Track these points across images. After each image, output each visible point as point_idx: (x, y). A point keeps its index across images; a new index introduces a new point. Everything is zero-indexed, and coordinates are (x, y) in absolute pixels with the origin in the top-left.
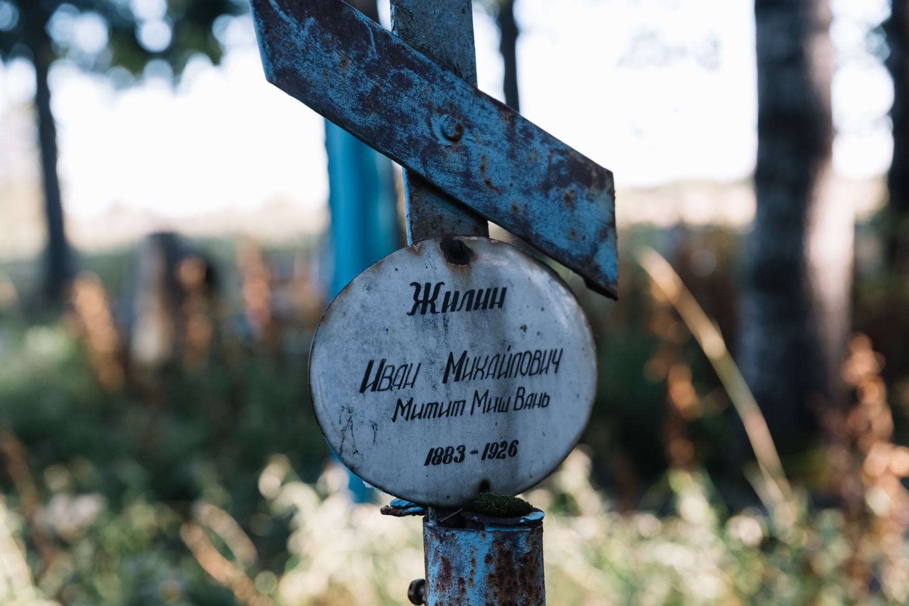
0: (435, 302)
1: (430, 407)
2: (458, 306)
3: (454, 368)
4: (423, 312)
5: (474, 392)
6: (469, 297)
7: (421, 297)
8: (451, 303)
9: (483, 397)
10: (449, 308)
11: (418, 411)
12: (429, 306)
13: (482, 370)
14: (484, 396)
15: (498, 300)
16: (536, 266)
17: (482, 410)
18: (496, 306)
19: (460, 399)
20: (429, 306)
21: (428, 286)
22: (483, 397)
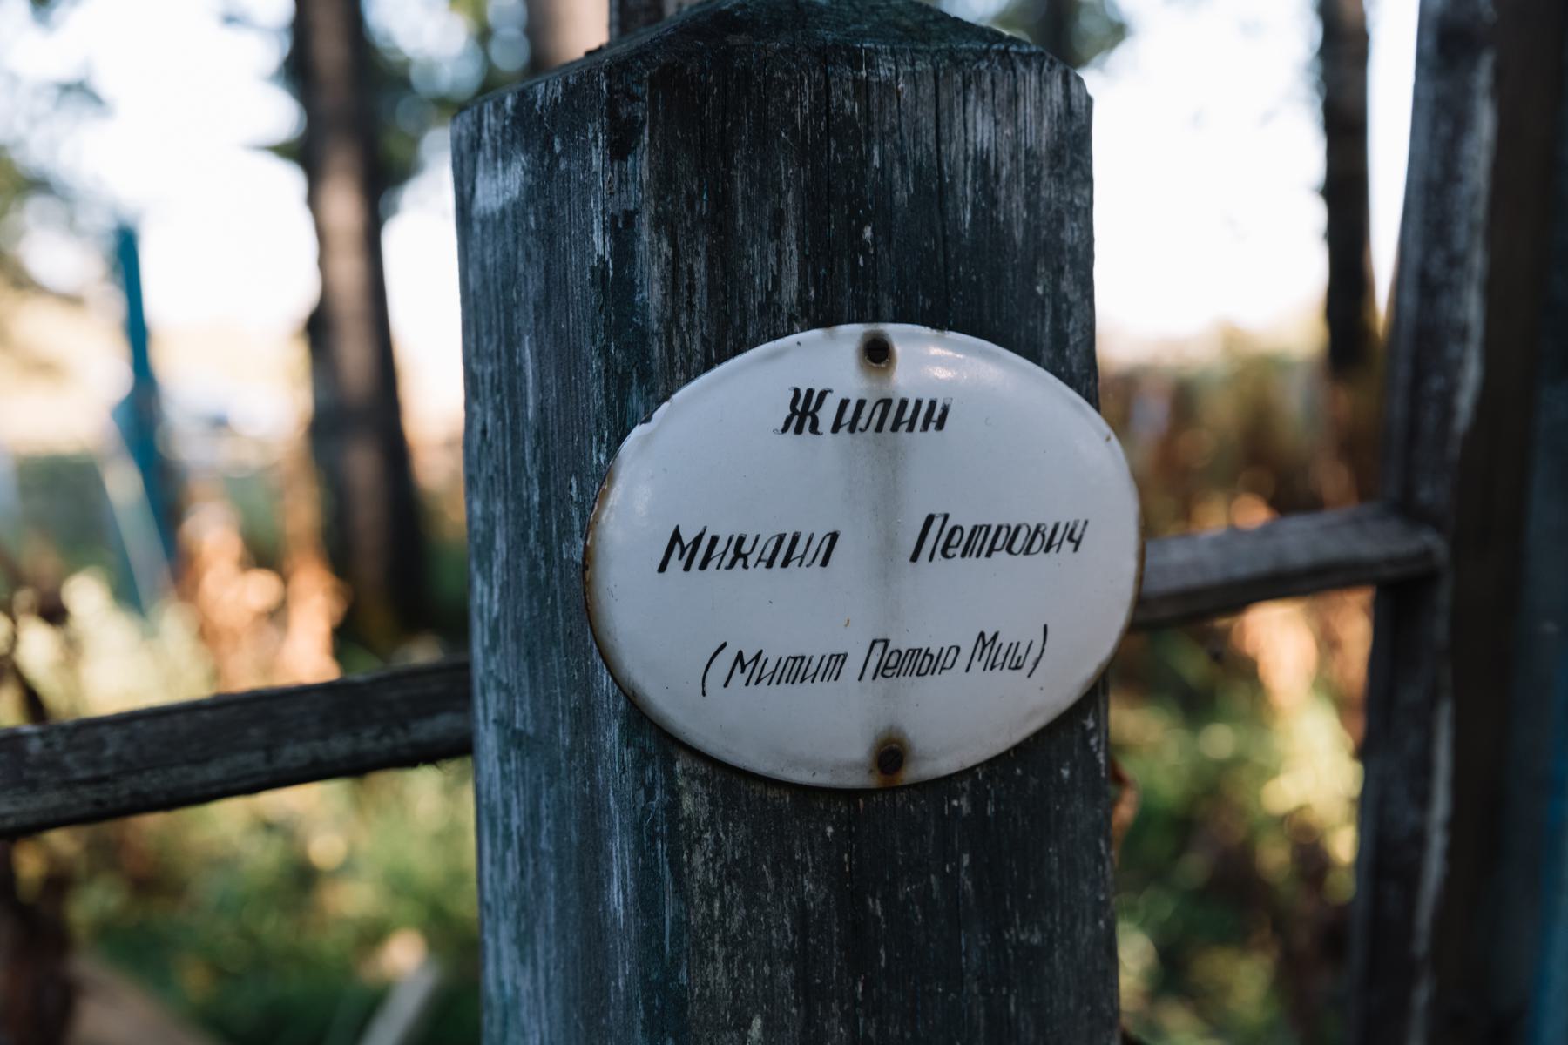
0: (817, 414)
1: (791, 661)
2: (862, 423)
3: (683, 550)
4: (799, 430)
5: (722, 643)
6: (808, 407)
7: (799, 407)
8: (850, 418)
9: (750, 662)
10: (905, 426)
11: (769, 668)
12: (808, 420)
13: (745, 557)
14: (752, 660)
15: (936, 416)
16: (120, 279)
17: (983, 667)
18: (932, 426)
19: (880, 637)
20: (808, 420)
21: (810, 392)
22: (750, 662)
